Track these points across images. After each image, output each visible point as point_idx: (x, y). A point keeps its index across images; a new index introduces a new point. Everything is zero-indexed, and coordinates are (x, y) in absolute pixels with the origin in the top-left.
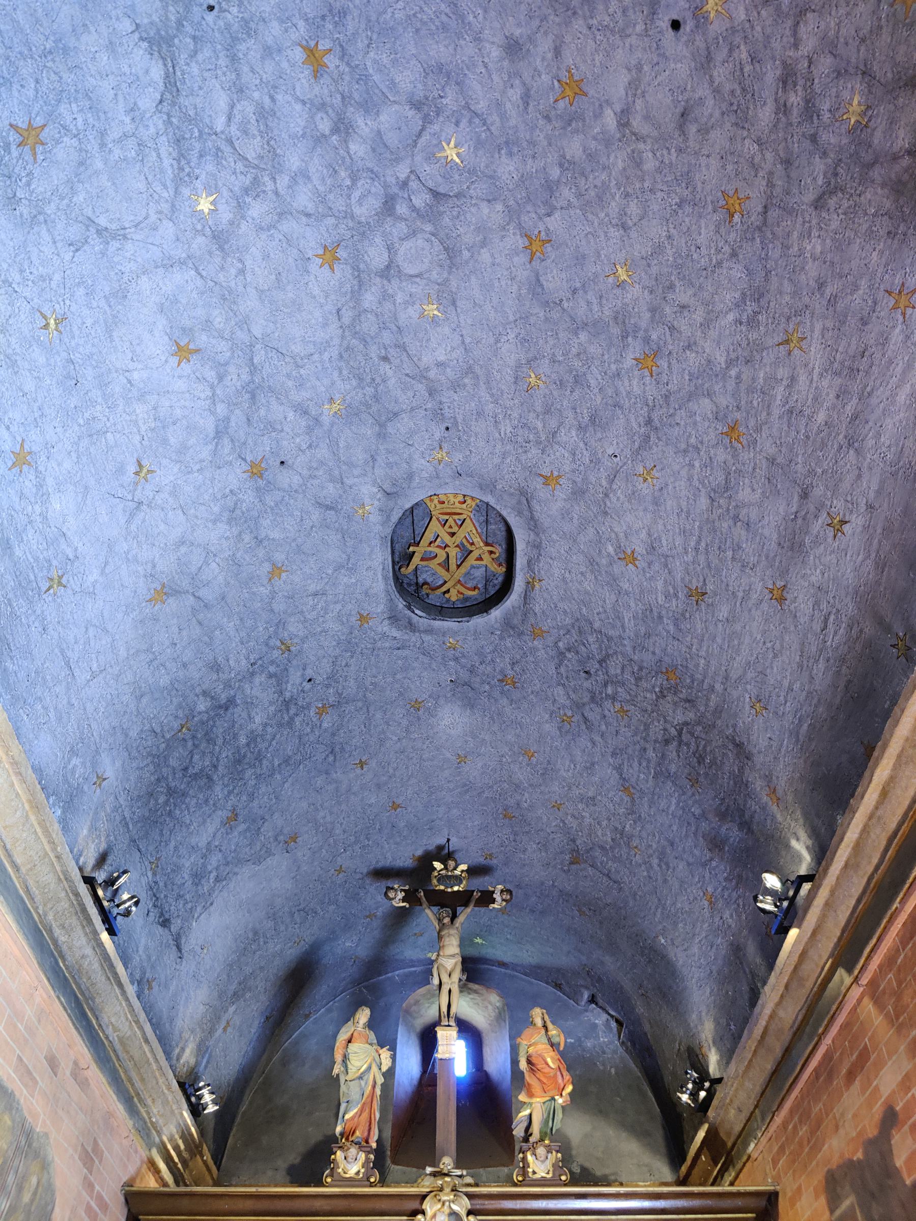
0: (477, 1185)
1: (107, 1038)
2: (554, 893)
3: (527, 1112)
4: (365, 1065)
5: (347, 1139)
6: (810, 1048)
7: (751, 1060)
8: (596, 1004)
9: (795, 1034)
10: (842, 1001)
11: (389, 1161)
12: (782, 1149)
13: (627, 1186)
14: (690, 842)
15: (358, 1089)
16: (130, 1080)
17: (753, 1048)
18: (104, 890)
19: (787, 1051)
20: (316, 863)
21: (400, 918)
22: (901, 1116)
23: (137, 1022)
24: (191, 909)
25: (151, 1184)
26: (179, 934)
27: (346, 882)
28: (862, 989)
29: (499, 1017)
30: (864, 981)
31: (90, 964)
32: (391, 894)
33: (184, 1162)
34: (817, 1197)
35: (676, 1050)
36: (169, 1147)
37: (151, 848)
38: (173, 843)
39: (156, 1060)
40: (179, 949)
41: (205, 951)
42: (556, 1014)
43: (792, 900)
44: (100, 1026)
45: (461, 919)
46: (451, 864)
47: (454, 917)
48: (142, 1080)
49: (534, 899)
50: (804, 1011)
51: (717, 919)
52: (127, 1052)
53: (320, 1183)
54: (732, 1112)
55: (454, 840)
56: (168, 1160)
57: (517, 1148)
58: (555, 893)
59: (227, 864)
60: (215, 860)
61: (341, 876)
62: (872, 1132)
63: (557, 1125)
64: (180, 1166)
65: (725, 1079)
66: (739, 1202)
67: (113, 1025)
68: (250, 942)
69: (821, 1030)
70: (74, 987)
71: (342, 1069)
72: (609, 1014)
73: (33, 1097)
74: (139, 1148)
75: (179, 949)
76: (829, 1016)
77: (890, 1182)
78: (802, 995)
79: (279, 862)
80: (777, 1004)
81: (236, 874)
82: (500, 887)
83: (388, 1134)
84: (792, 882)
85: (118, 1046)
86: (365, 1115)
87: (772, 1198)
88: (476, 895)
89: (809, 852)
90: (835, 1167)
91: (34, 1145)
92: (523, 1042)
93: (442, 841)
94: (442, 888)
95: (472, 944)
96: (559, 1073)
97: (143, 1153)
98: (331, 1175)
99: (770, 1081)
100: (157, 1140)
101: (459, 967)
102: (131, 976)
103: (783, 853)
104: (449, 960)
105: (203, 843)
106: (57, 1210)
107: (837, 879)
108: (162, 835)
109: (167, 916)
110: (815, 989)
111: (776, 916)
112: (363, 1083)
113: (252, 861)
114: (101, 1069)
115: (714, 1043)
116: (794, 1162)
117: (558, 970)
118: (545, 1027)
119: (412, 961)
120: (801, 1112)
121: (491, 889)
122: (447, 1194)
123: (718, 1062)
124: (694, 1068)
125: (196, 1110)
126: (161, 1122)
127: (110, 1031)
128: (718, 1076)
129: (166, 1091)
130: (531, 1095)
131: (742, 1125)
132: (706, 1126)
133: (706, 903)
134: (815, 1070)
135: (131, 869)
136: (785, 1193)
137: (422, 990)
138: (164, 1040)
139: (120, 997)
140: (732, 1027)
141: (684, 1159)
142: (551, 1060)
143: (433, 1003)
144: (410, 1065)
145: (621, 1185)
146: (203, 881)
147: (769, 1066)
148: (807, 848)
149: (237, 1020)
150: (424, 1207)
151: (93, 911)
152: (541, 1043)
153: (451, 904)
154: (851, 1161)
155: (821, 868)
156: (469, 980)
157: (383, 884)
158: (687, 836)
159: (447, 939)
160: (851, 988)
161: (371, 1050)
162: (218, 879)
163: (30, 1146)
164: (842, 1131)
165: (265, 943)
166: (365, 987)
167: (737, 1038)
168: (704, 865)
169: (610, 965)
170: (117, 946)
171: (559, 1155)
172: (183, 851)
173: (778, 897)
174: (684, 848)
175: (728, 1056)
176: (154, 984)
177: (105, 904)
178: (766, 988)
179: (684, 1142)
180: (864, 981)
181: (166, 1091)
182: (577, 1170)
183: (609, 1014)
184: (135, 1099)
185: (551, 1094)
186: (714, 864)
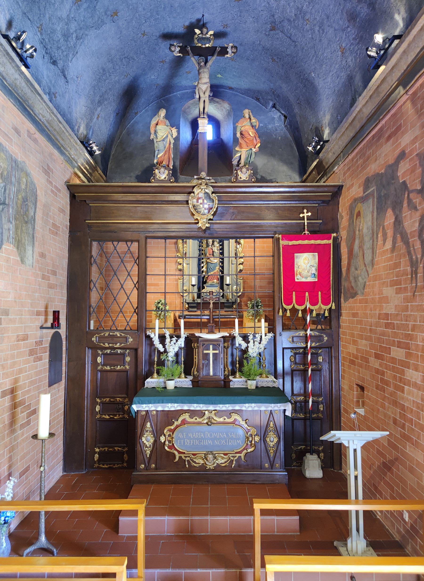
0: (216, 183)
1: (40, 120)
2: (260, 48)
3: (239, 155)
4: (164, 135)
5: (159, 165)
6: (374, 126)
7: (344, 132)
8: (276, 108)
9: (368, 119)
10: (396, 103)
11: (179, 174)
12: (349, 169)
13: (280, 183)
14: (338, 16)
15: (163, 145)
16: (57, 140)
17: (347, 126)
18: (16, 43)
19: (362, 127)
20: (130, 29)
21: (178, 63)
22: (407, 155)
23: (53, 113)
24: (66, 55)
25: (78, 182)
26: (63, 69)
27: (148, 41)
28: (408, 96)
29: (229, 115)
30: (410, 93)
31: (20, 83)
32: (173, 49)
33: (90, 174)
34: (359, 188)
35: (310, 129)
36: (82, 168)
37: (36, 18)
38: (47, 16)
39: (67, 131)
40: (65, 78)
41: (79, 79)
42: (255, 113)
43: (386, 50)
44: (35, 114)
45: (210, 63)
46: (205, 30)
47: (206, 62)
48: (63, 140)
49: (249, 52)
50: (375, 109)
51: (344, 62)
52: (53, 127)
53: (150, 182)
54: (331, 154)
55: (206, 16)
56: (83, 173)
57: (234, 169)
58: (260, 48)
59: (81, 29)
60: (73, 26)
61: (145, 37)
62: (391, 161)
63: (252, 159)
64: (88, 175)
65: (330, 141)
66: (326, 189)
67: (41, 114)
68: (102, 75)
69: (381, 117)
70: (16, 95)
71: (155, 136)
72: (281, 113)
73: (12, 146)
74: (69, 168)
75: (65, 78)
76: (387, 110)
77: (393, 182)
78: (377, 100)
79: (109, 28)
80: (364, 105)
81: (87, 35)
82: (231, 45)
83: (178, 163)
84: (389, 40)
85: (47, 124)
86: (167, 156)
87: (340, 188)
88: (218, 49)
89: (403, 22)
90: (370, 176)
91: (20, 166)
92: (239, 125)
93: (199, 16)
94: (200, 45)
95: (216, 77)
96: (254, 139)
97: (71, 170)
98: (154, 179)
99: (350, 141)
100: (76, 165)
101: (209, 89)
102: (44, 90)
103: (389, 22)
104: (204, 86)
105: (64, 16)
106: (38, 191)
107: (414, 37)
108: (40, 10)
109: (54, 59)
110: (384, 97)
111: (376, 59)
112: (165, 142)
113: (94, 27)
114: (42, 135)
115: (328, 125)
116: (353, 174)
117: (258, 92)
118: (250, 118)
119: (186, 86)
120: (362, 153)
121: (226, 46)
122: (203, 186)
123: (329, 134)
124: (317, 136)
125: (91, 153)
126: (76, 158)
127: (41, 117)
128: (327, 139)
129: (75, 145)
130: (241, 148)
131: (334, 159)
132: (318, 160)
133: (340, 53)
134: (373, 135)
135: (28, 30)
136: (346, 186)
137: (191, 102)
138: (69, 122)
139: (41, 101)
140: (339, 117)
141: (305, 173)
142: (252, 133)
143: (197, 108)
144: (186, 136)
145: (277, 183)
146: (70, 39)
147: (352, 135)
148: (403, 19)
149: (103, 114)
150: (194, 191)
151: (13, 55)
152: (247, 125)
153: (204, 54)
154: (378, 173)
155: (407, 31)
156: (214, 96)
157: (168, 43)
158: (337, 12)
159: (203, 74)
160: (402, 96)
161: (168, 129)
162: (77, 38)
163: (18, 166)
164: (378, 162)
165: (110, 76)
166: (164, 100)
167: (340, 122)
168: (343, 30)
169: (285, 89)
170: (32, 75)
171: (252, 171)
172: (54, 20)
173: (379, 48)
174: (334, 20)
175: (333, 130)
176: (57, 95)
177: (19, 51)
178: (360, 98)
179: (307, 167)
180: (410, 93)
181: (75, 145)
182: (259, 177)
183: (281, 113)
184: (62, 148)
185: (250, 147)
186: (349, 29)
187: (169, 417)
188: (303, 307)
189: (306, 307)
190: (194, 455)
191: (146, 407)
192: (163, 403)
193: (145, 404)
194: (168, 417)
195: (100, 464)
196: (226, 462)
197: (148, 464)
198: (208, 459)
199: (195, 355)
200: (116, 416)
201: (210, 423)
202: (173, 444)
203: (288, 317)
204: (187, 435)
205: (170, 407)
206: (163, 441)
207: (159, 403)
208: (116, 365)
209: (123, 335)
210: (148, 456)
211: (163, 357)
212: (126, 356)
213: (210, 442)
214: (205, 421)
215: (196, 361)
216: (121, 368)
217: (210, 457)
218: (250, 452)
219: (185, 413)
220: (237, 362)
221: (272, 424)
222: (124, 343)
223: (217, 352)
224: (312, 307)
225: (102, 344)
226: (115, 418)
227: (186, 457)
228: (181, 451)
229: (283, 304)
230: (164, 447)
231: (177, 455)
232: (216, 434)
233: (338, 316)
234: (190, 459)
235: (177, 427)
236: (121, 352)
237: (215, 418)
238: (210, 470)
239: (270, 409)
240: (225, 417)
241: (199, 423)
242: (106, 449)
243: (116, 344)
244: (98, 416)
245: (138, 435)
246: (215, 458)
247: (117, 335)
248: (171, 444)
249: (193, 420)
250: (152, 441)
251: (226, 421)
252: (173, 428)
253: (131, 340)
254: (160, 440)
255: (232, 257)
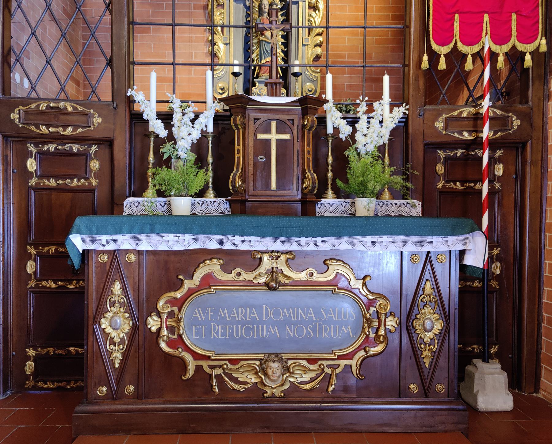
187: (171, 270)
188: (476, 48)
189: (483, 47)
190: (233, 362)
191: (108, 241)
192: (152, 232)
193: (107, 234)
194: (167, 270)
195: (37, 382)
196: (312, 380)
197: (117, 385)
198: (270, 372)
199: (238, 145)
200: (71, 283)
201: (273, 284)
202: (180, 336)
203: (441, 71)
204: (215, 312)
205: (171, 243)
206: (154, 329)
207: (142, 232)
208: (69, 178)
209: (80, 108)
210: (117, 366)
211: (167, 150)
212: (92, 159)
213: (275, 331)
214: (262, 280)
215: (238, 158)
216: (80, 183)
217: (275, 367)
218: (375, 355)
219: (211, 259)
220: (330, 168)
221: (428, 288)
222: (83, 127)
223: (287, 137)
224: (496, 48)
225: (33, 128)
226: (69, 286)
227: (212, 367)
228: (199, 351)
229: (432, 43)
230: (158, 344)
231: (192, 364)
232: (288, 310)
233: (545, 74)
234: (225, 373)
235: (191, 292)
236: (78, 150)
237: (287, 271)
238: (273, 398)
239: (427, 248)
240: (313, 271)
241: (250, 285)
242: (51, 351)
243: (65, 127)
244: (32, 284)
245: (91, 315)
246: (286, 369)
247: (65, 108)
248: (175, 337)
249: (231, 277)
250: (126, 326)
251: (314, 278)
252: (179, 296)
253: (97, 120)
254: (146, 325)
255: (303, 27)
